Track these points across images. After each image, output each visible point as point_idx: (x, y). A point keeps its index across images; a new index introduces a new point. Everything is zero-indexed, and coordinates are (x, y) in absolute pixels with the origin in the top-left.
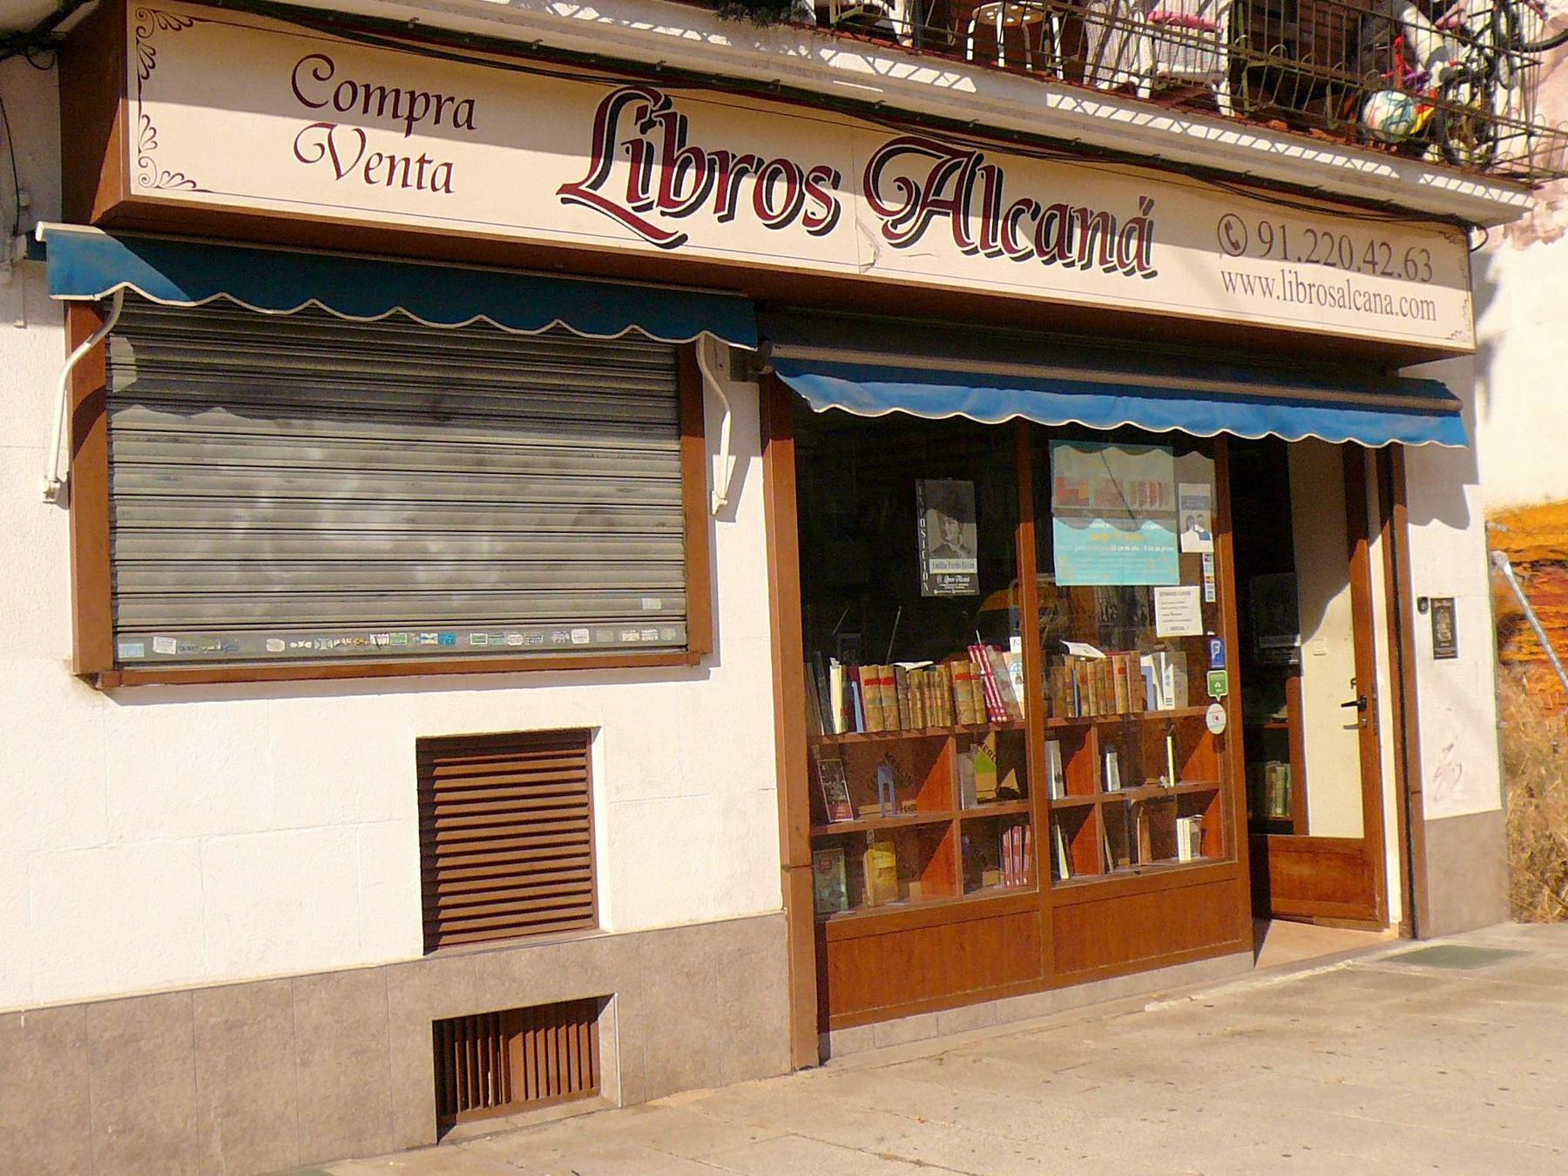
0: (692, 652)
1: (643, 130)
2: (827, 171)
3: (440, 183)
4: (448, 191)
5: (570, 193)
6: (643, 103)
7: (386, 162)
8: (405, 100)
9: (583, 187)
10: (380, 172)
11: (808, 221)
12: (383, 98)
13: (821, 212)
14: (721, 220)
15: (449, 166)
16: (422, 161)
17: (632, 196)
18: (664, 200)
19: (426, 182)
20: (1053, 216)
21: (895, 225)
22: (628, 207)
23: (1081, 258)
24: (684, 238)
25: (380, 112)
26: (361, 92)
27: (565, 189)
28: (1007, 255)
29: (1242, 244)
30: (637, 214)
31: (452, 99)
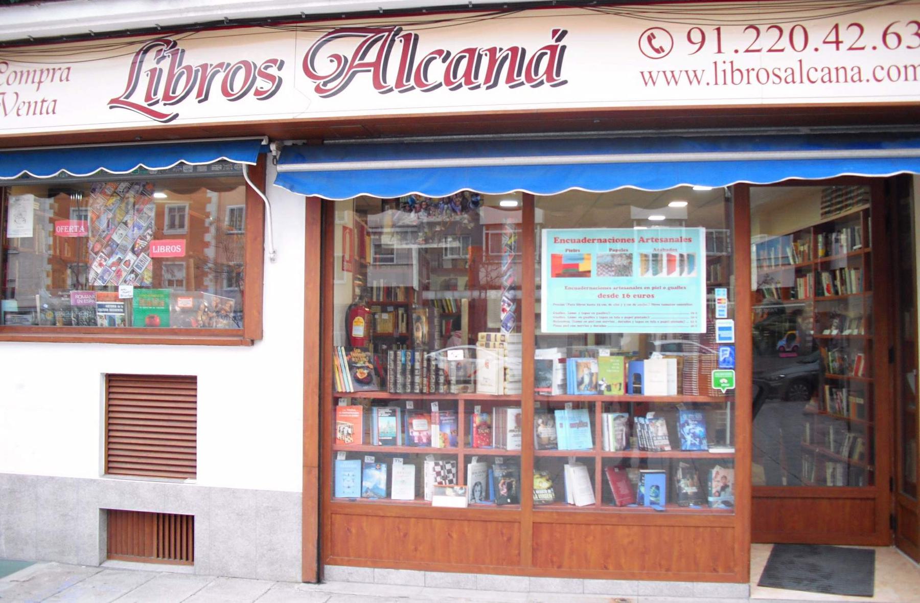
0: (243, 329)
1: (158, 63)
2: (274, 61)
3: (50, 110)
4: (54, 113)
5: (115, 103)
6: (159, 48)
7: (27, 105)
8: (910, 70)
9: (122, 99)
10: (23, 111)
11: (257, 93)
12: (28, 74)
13: (267, 85)
14: (200, 102)
15: (55, 101)
16: (43, 101)
17: (148, 98)
18: (166, 97)
19: (44, 111)
20: (462, 58)
21: (325, 84)
22: (145, 105)
23: (487, 80)
24: (177, 115)
25: (26, 82)
26: (19, 75)
27: (113, 101)
28: (418, 89)
29: (667, 50)
30: (152, 108)
31: (753, 70)
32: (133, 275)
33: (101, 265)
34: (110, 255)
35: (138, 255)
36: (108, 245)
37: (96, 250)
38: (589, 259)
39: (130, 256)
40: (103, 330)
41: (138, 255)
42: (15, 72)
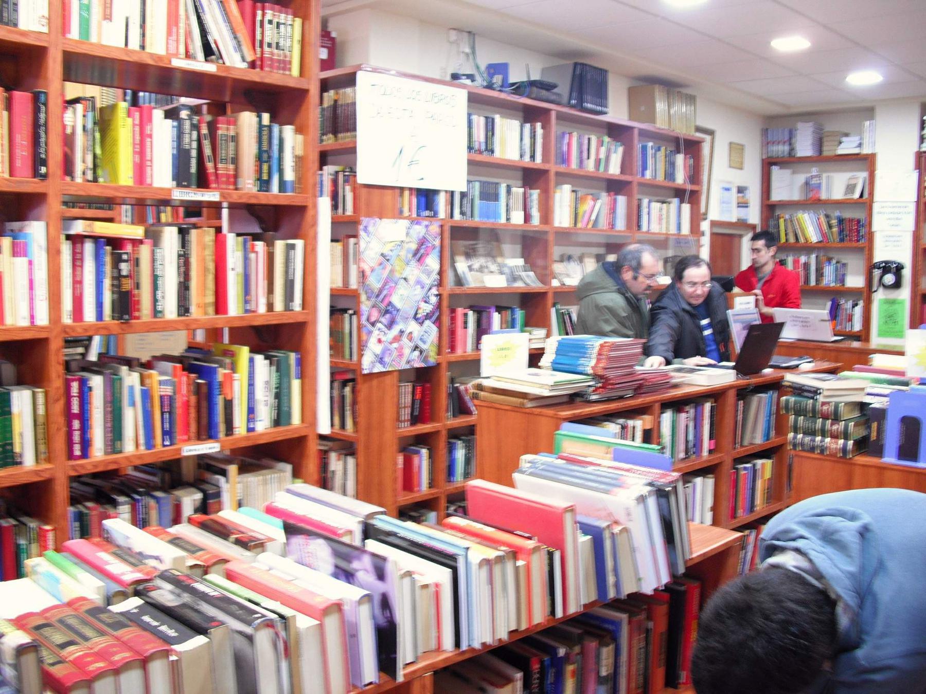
32: (417, 353)
33: (380, 341)
34: (390, 326)
35: (421, 324)
36: (387, 312)
37: (373, 319)
38: (384, 559)
39: (413, 327)
40: (229, 461)
41: (421, 324)
42: (742, 446)
